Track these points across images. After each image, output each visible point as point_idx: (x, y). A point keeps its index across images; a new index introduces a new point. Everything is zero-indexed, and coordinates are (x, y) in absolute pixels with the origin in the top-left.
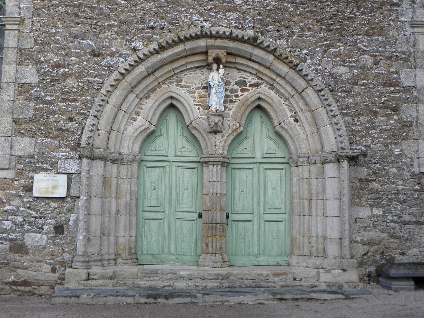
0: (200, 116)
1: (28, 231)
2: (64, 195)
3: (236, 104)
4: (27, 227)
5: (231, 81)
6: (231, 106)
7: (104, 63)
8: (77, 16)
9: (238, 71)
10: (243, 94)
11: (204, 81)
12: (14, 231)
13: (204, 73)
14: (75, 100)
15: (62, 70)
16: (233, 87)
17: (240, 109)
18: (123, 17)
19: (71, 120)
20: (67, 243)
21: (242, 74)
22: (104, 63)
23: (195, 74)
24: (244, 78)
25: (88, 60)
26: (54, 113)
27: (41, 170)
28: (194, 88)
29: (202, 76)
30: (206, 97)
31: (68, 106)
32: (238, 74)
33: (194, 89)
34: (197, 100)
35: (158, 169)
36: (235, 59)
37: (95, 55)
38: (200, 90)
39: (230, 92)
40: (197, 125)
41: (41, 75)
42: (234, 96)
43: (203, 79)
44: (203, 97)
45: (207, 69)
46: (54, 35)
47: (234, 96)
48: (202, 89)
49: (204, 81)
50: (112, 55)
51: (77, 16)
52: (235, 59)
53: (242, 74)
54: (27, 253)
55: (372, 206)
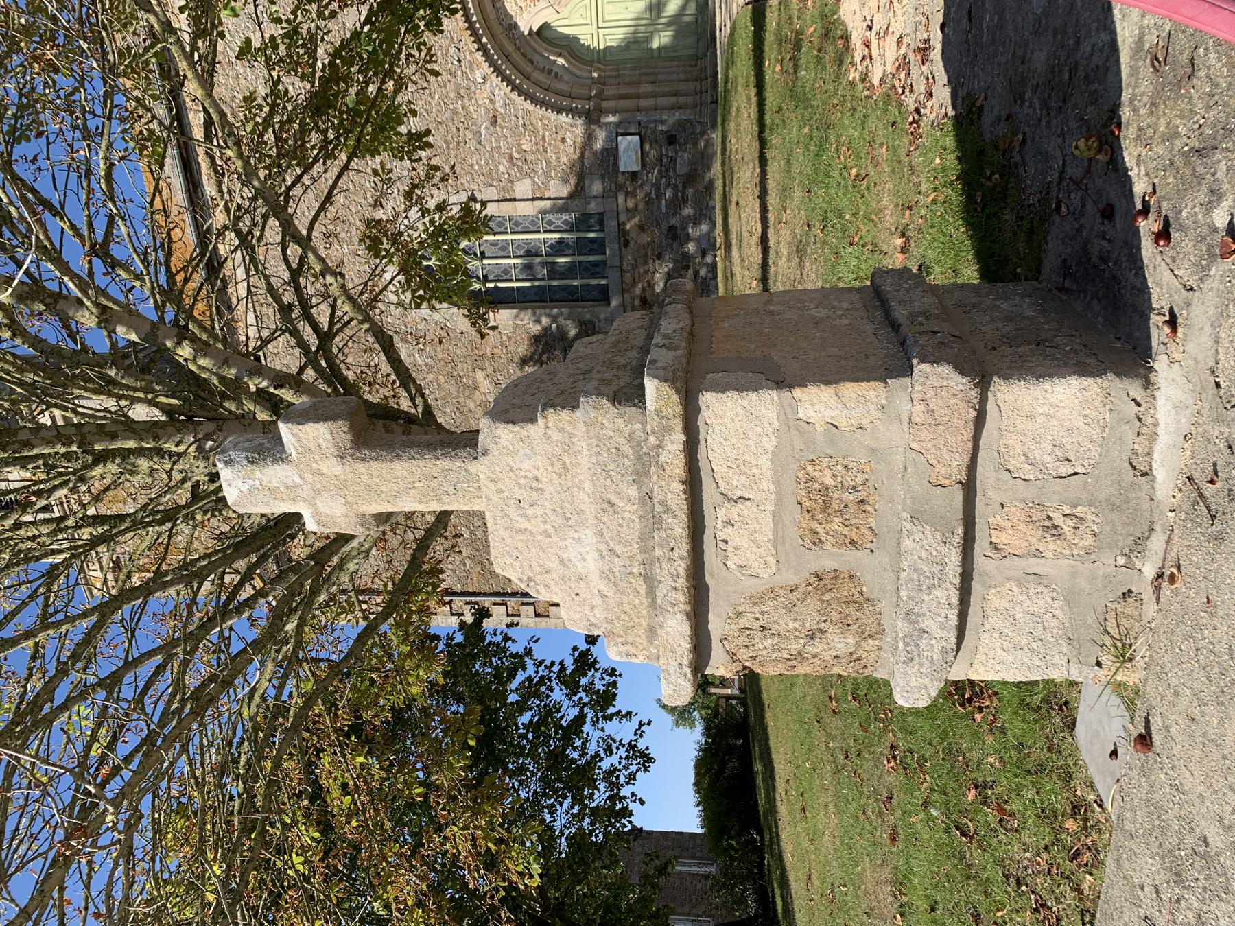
1: (675, 171)
2: (637, 138)
4: (671, 174)
7: (502, 111)
8: (458, 144)
12: (675, 186)
14: (544, 139)
15: (515, 155)
18: (452, 95)
19: (563, 140)
20: (685, 130)
22: (502, 111)
25: (502, 128)
26: (558, 159)
27: (616, 165)
31: (550, 144)
35: (980, 562)
37: (496, 121)
41: (523, 175)
46: (481, 166)
50: (492, 101)
51: (458, 144)
54: (696, 170)
55: (103, 525)
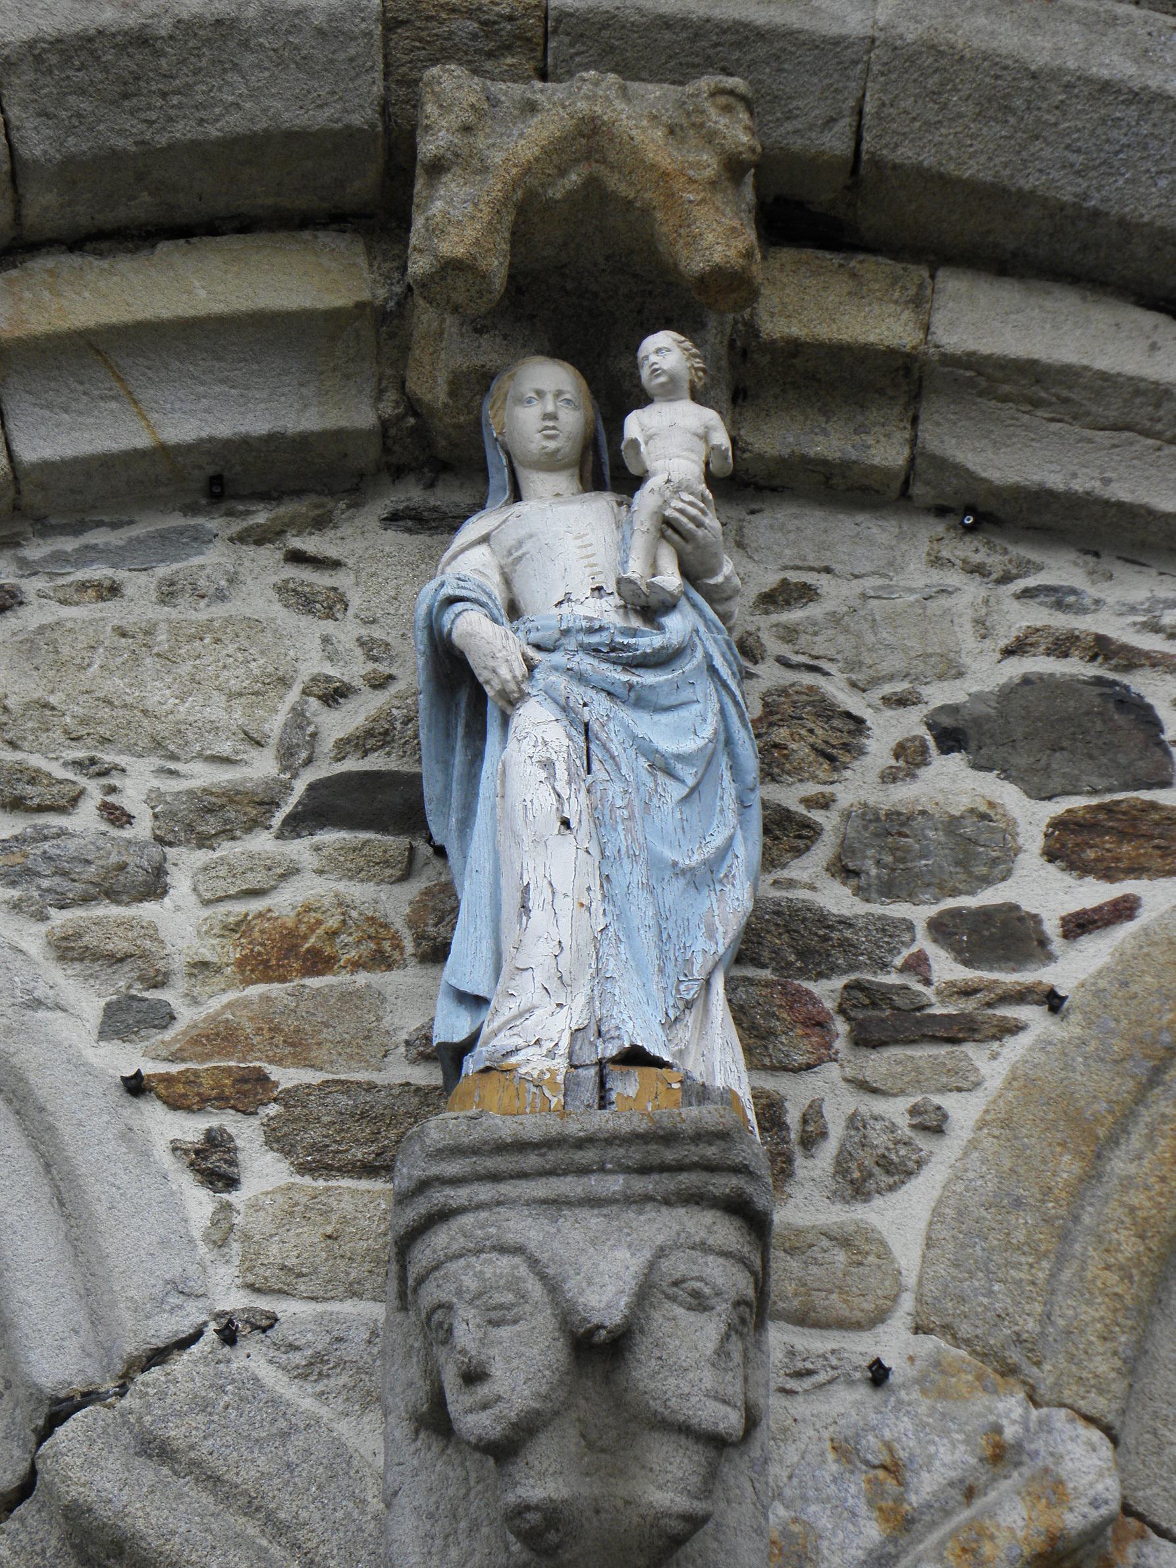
0: (235, 1301)
3: (1015, 1048)
5: (852, 703)
6: (896, 1110)
9: (972, 550)
10: (1124, 909)
11: (335, 695)
13: (342, 580)
16: (903, 794)
17: (1093, 1175)
21: (1059, 598)
23: (168, 593)
24: (1101, 648)
28: (132, 797)
29: (313, 628)
30: (381, 961)
32: (971, 591)
33: (143, 828)
34: (187, 1016)
36: (920, 303)
38: (262, 842)
39: (844, 870)
40: (149, 1472)
42: (940, 928)
43: (313, 664)
44: (319, 963)
45: (393, 519)
47: (940, 928)
48: (297, 824)
49: (335, 695)
52: (920, 303)
53: (1059, 598)
